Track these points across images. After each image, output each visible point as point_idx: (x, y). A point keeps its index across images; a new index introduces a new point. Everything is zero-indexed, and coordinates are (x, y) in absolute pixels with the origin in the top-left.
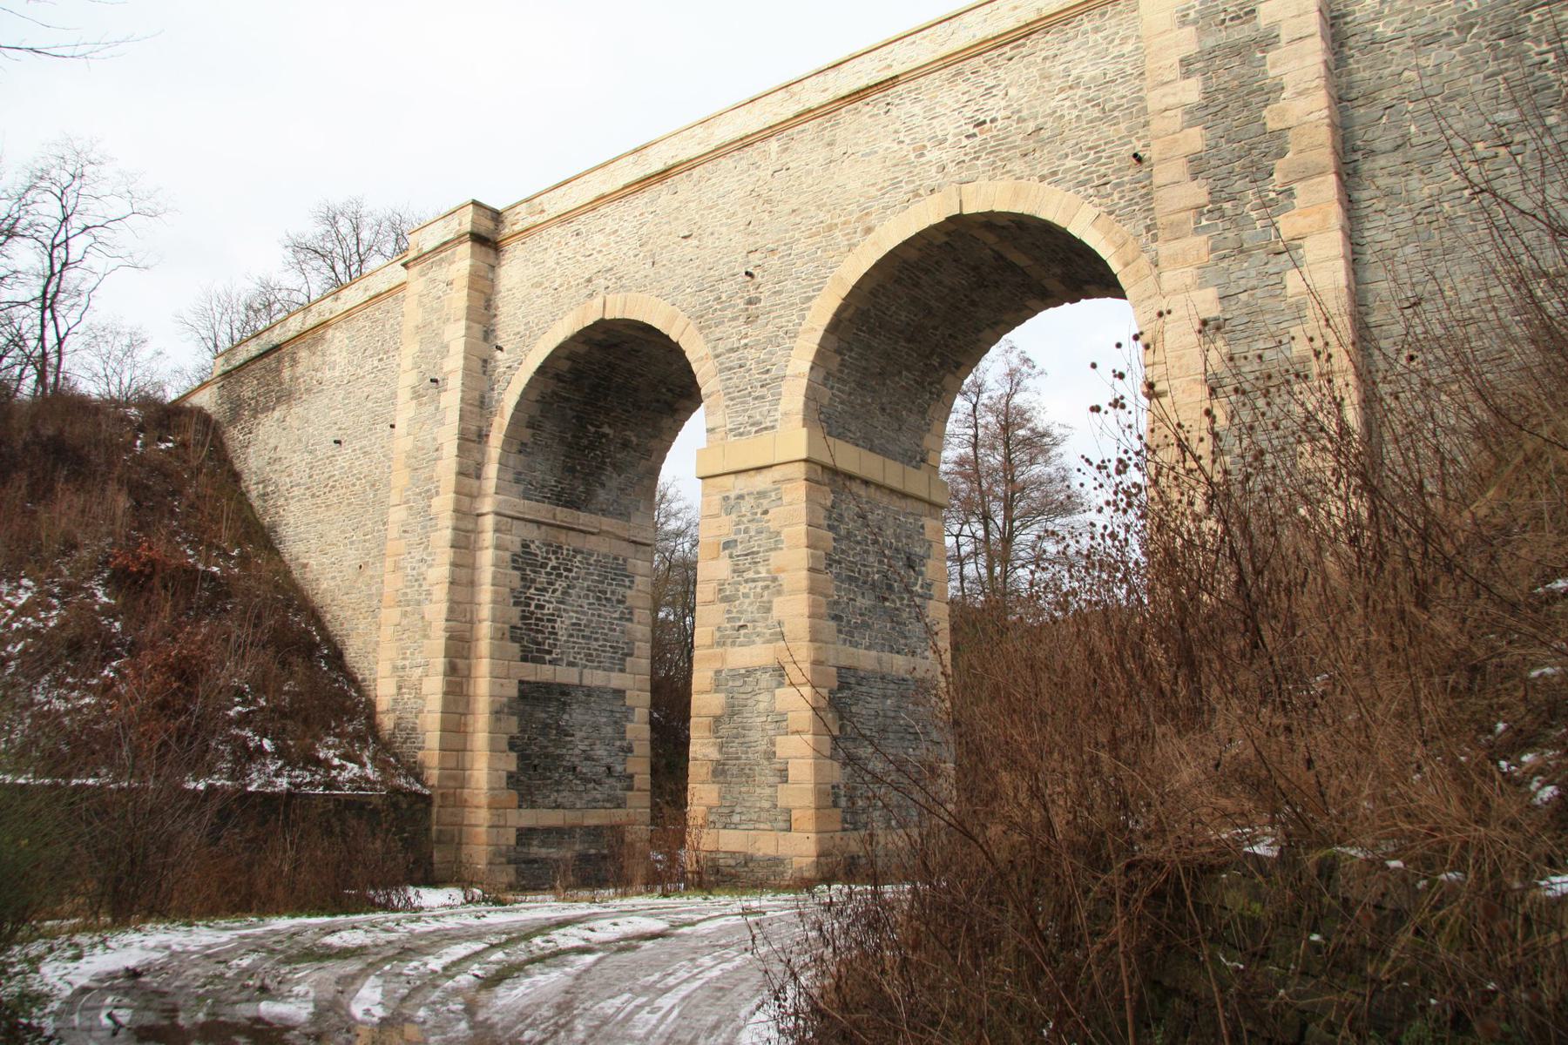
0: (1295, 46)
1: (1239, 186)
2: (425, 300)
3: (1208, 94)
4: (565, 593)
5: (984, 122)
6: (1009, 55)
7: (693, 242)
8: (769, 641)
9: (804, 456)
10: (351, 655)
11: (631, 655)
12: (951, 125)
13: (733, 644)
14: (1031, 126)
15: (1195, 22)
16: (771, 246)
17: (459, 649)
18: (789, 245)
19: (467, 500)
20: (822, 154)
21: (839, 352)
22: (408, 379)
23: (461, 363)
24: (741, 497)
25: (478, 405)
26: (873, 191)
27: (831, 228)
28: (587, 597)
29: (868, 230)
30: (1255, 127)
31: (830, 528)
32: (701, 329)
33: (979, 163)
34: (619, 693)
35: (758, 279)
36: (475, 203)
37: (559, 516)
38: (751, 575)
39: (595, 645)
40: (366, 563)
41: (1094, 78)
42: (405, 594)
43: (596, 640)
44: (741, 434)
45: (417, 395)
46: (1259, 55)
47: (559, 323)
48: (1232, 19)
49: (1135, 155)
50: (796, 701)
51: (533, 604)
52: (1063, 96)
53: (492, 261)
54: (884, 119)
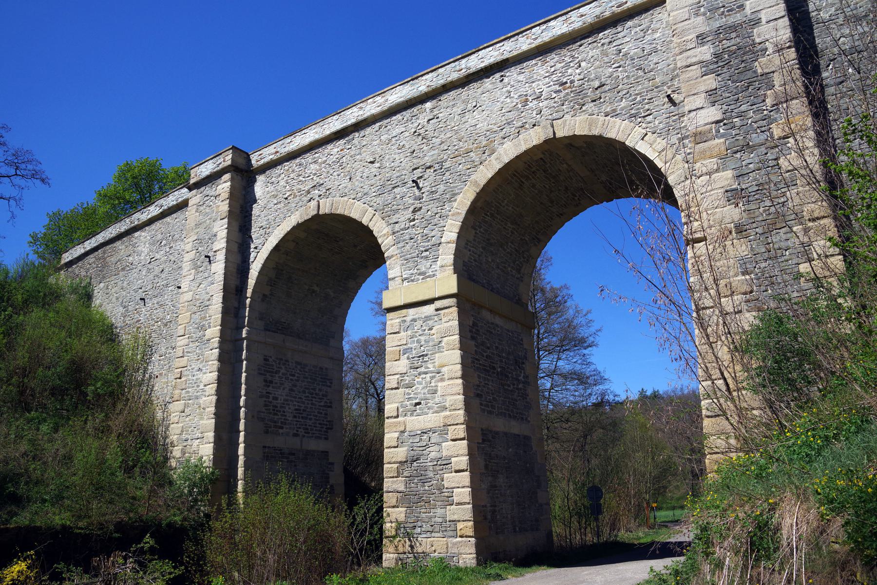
0: (772, 24)
1: (744, 108)
3: (718, 56)
4: (291, 390)
5: (566, 83)
7: (377, 165)
8: (436, 412)
9: (454, 290)
11: (331, 429)
12: (544, 86)
13: (412, 415)
14: (597, 84)
15: (704, 14)
16: (428, 164)
18: (441, 163)
21: (473, 227)
23: (224, 245)
24: (414, 320)
26: (495, 128)
28: (304, 392)
30: (749, 74)
31: (473, 338)
33: (564, 107)
34: (325, 453)
36: (234, 148)
38: (423, 369)
39: (309, 422)
43: (310, 419)
44: (412, 281)
49: (668, 96)
50: (458, 453)
54: (500, 85)
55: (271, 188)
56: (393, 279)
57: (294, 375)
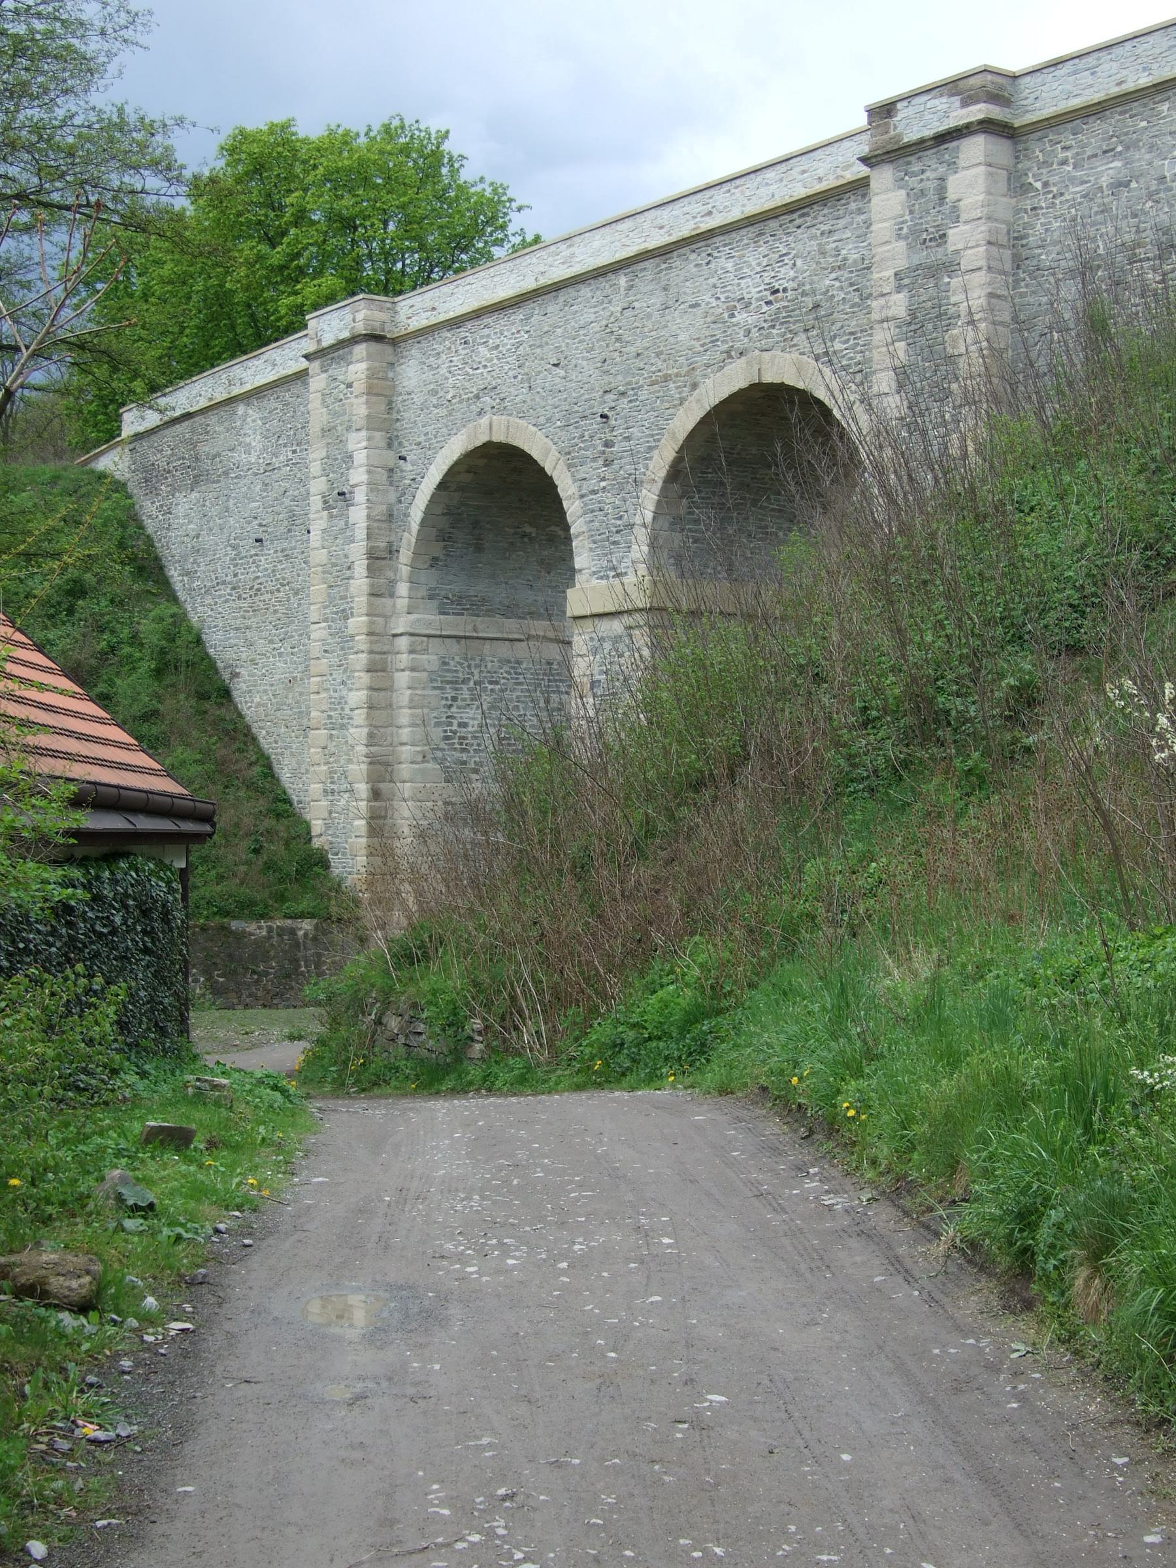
2: (329, 400)
6: (798, 222)
7: (560, 372)
10: (285, 775)
12: (753, 289)
16: (621, 388)
17: (381, 771)
19: (380, 620)
20: (657, 300)
22: (318, 486)
25: (388, 519)
27: (667, 378)
29: (695, 386)
32: (569, 466)
33: (774, 331)
35: (612, 422)
37: (480, 627)
40: (295, 678)
41: (855, 261)
42: (330, 717)
45: (327, 506)
46: (947, 280)
47: (454, 438)
48: (931, 240)
51: (455, 722)
52: (833, 276)
53: (391, 359)
55: (428, 376)
56: (580, 571)
57: (497, 683)
